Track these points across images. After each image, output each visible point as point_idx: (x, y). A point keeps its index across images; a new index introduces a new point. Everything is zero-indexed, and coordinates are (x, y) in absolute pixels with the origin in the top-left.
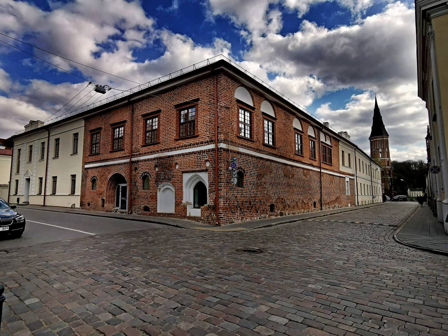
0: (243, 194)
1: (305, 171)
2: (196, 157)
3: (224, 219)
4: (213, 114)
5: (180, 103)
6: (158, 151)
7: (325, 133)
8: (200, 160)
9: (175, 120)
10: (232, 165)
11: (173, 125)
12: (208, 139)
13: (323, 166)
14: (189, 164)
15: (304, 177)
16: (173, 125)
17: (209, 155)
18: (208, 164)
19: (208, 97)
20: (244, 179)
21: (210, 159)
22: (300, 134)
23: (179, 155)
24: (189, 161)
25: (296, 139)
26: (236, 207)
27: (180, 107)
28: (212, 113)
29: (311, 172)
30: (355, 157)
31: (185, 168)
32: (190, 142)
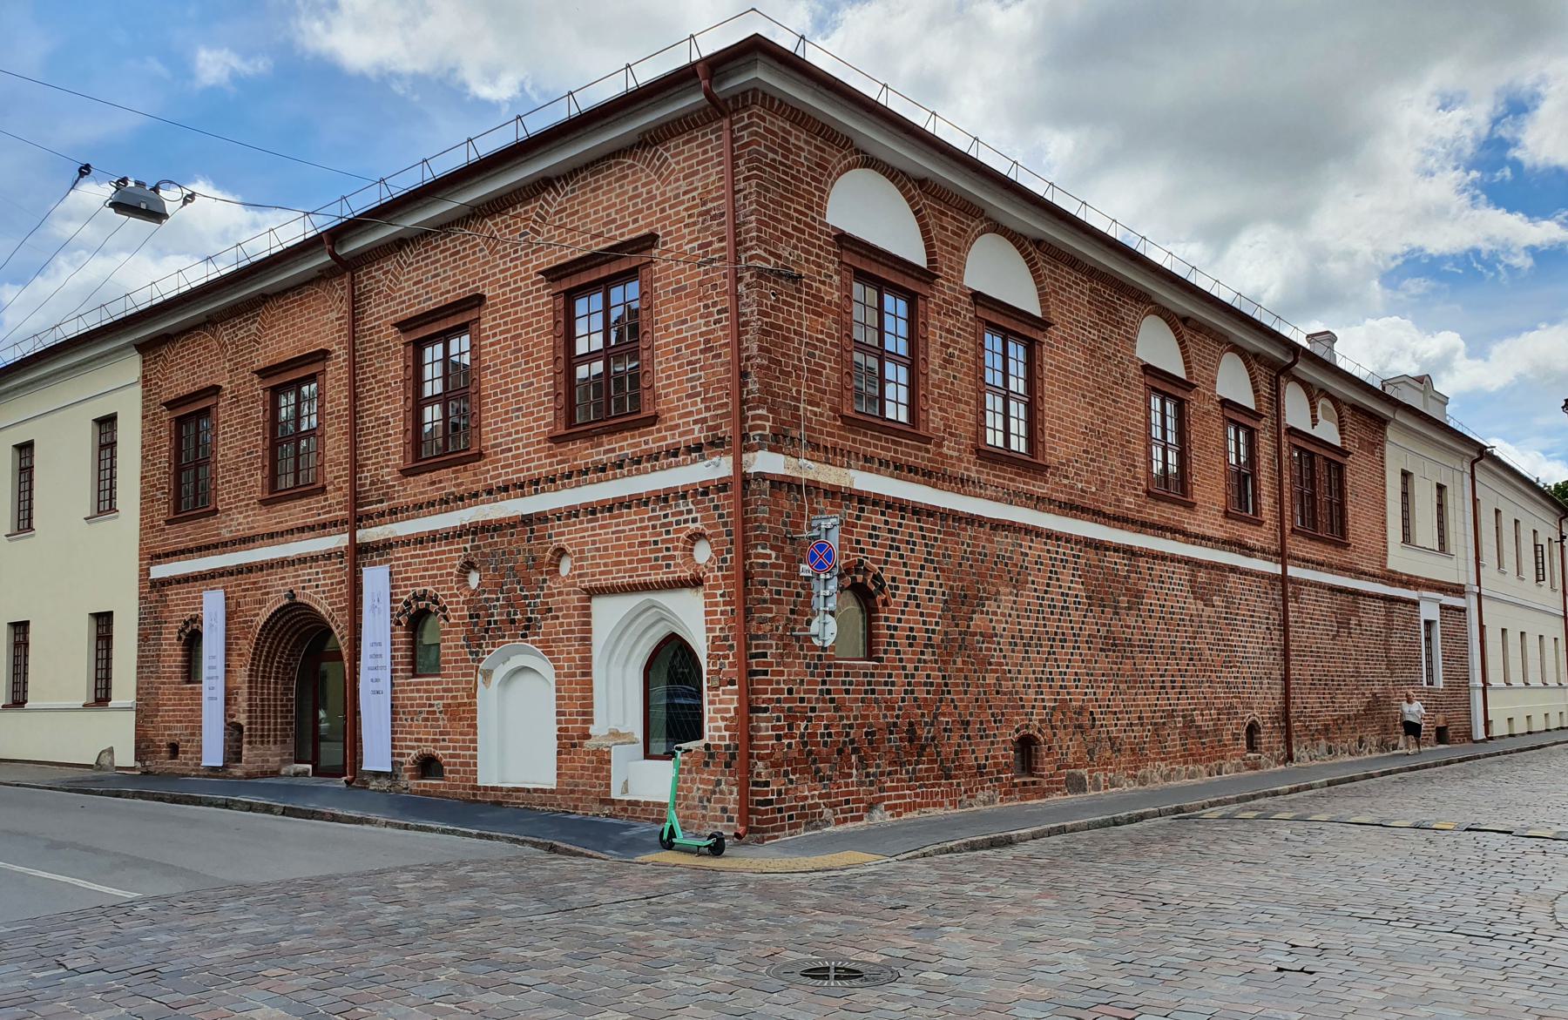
0: (873, 691)
1: (1202, 576)
2: (650, 519)
3: (780, 810)
4: (719, 312)
5: (570, 258)
6: (476, 495)
7: (1306, 386)
8: (668, 532)
9: (547, 341)
10: (813, 557)
11: (538, 367)
12: (701, 431)
13: (1297, 546)
14: (618, 555)
15: (1195, 606)
16: (538, 367)
17: (706, 509)
18: (703, 553)
19: (694, 224)
20: (878, 619)
21: (709, 526)
22: (1172, 397)
23: (572, 512)
24: (618, 539)
25: (1156, 418)
26: (840, 752)
27: (573, 280)
28: (715, 304)
29: (1232, 577)
30: (1475, 501)
31: (601, 573)
32: (622, 448)
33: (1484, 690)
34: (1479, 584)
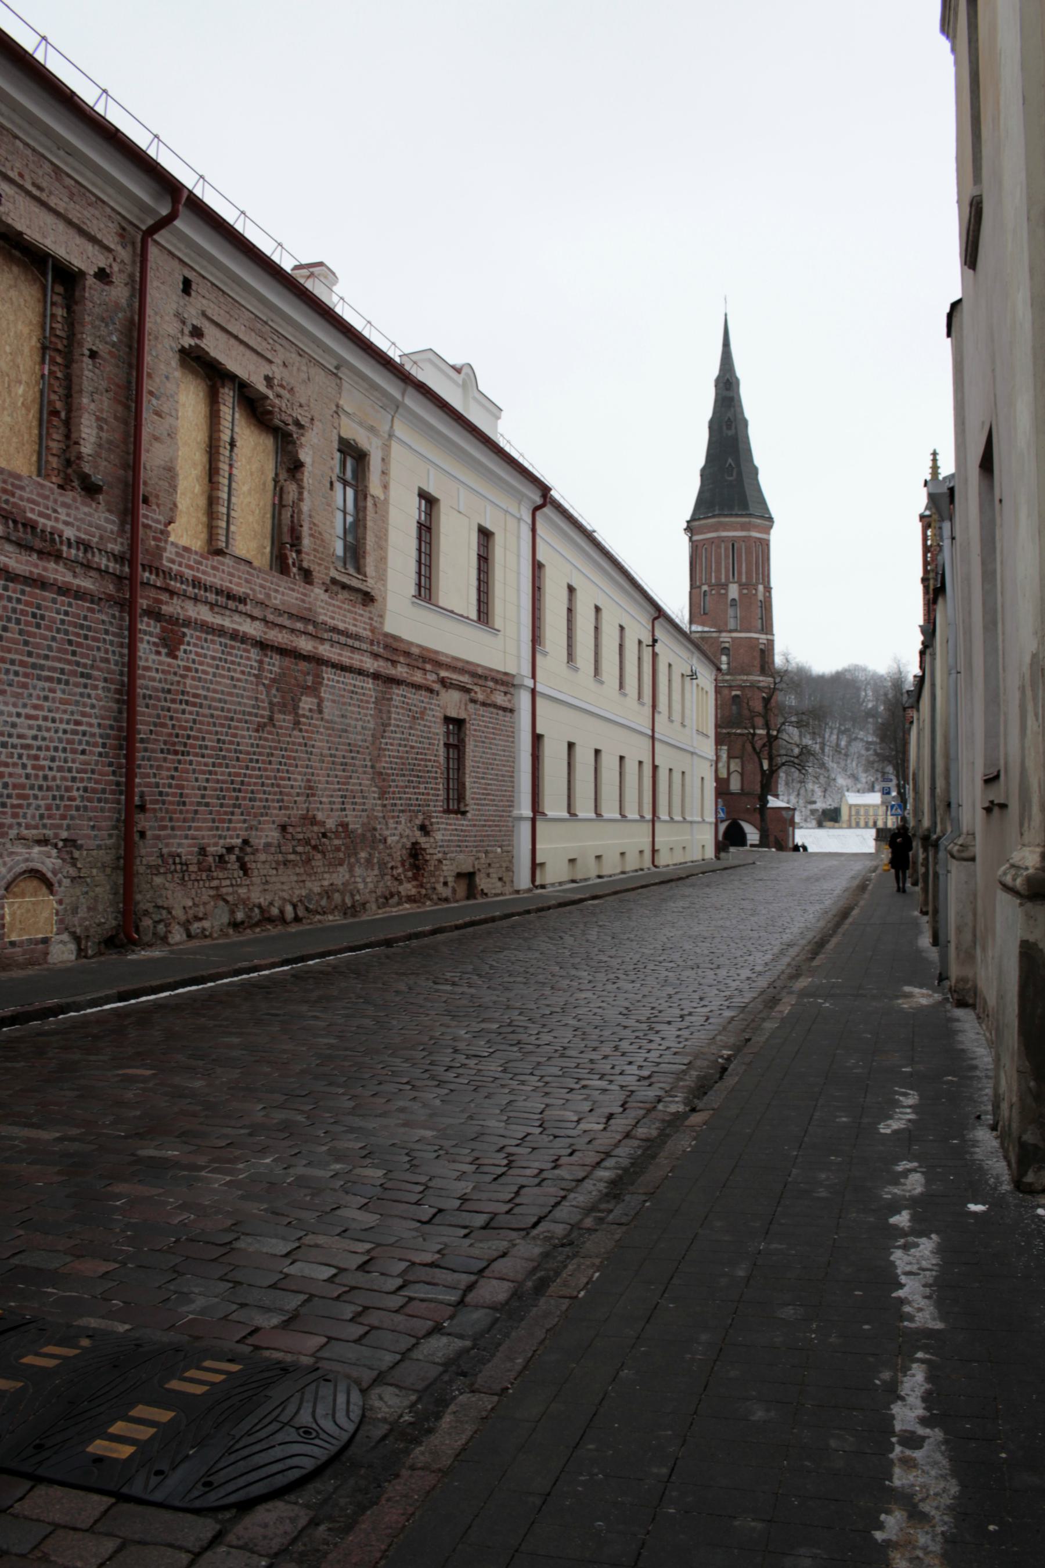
30: (537, 567)
33: (534, 821)
34: (534, 676)
